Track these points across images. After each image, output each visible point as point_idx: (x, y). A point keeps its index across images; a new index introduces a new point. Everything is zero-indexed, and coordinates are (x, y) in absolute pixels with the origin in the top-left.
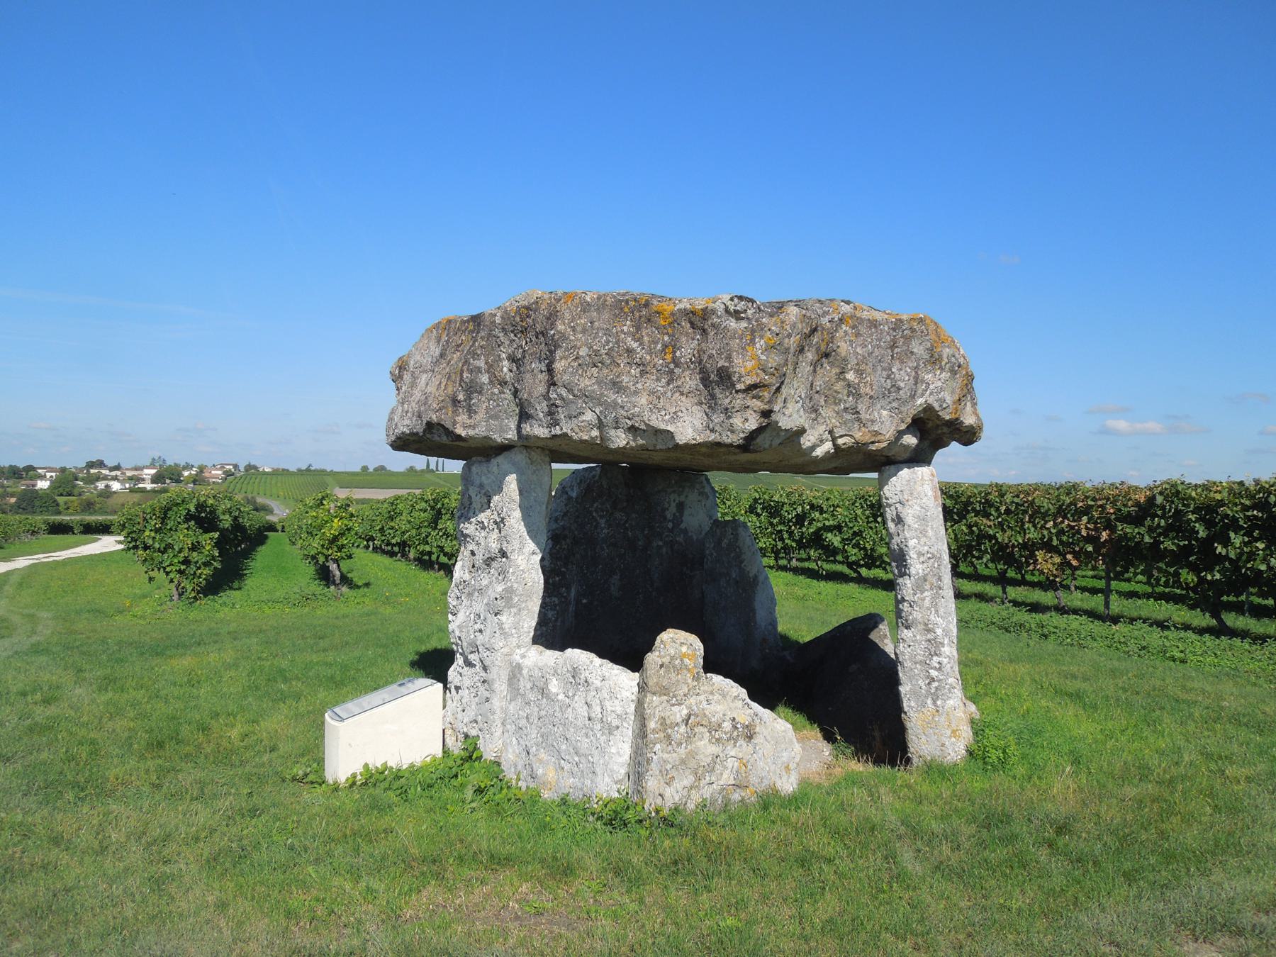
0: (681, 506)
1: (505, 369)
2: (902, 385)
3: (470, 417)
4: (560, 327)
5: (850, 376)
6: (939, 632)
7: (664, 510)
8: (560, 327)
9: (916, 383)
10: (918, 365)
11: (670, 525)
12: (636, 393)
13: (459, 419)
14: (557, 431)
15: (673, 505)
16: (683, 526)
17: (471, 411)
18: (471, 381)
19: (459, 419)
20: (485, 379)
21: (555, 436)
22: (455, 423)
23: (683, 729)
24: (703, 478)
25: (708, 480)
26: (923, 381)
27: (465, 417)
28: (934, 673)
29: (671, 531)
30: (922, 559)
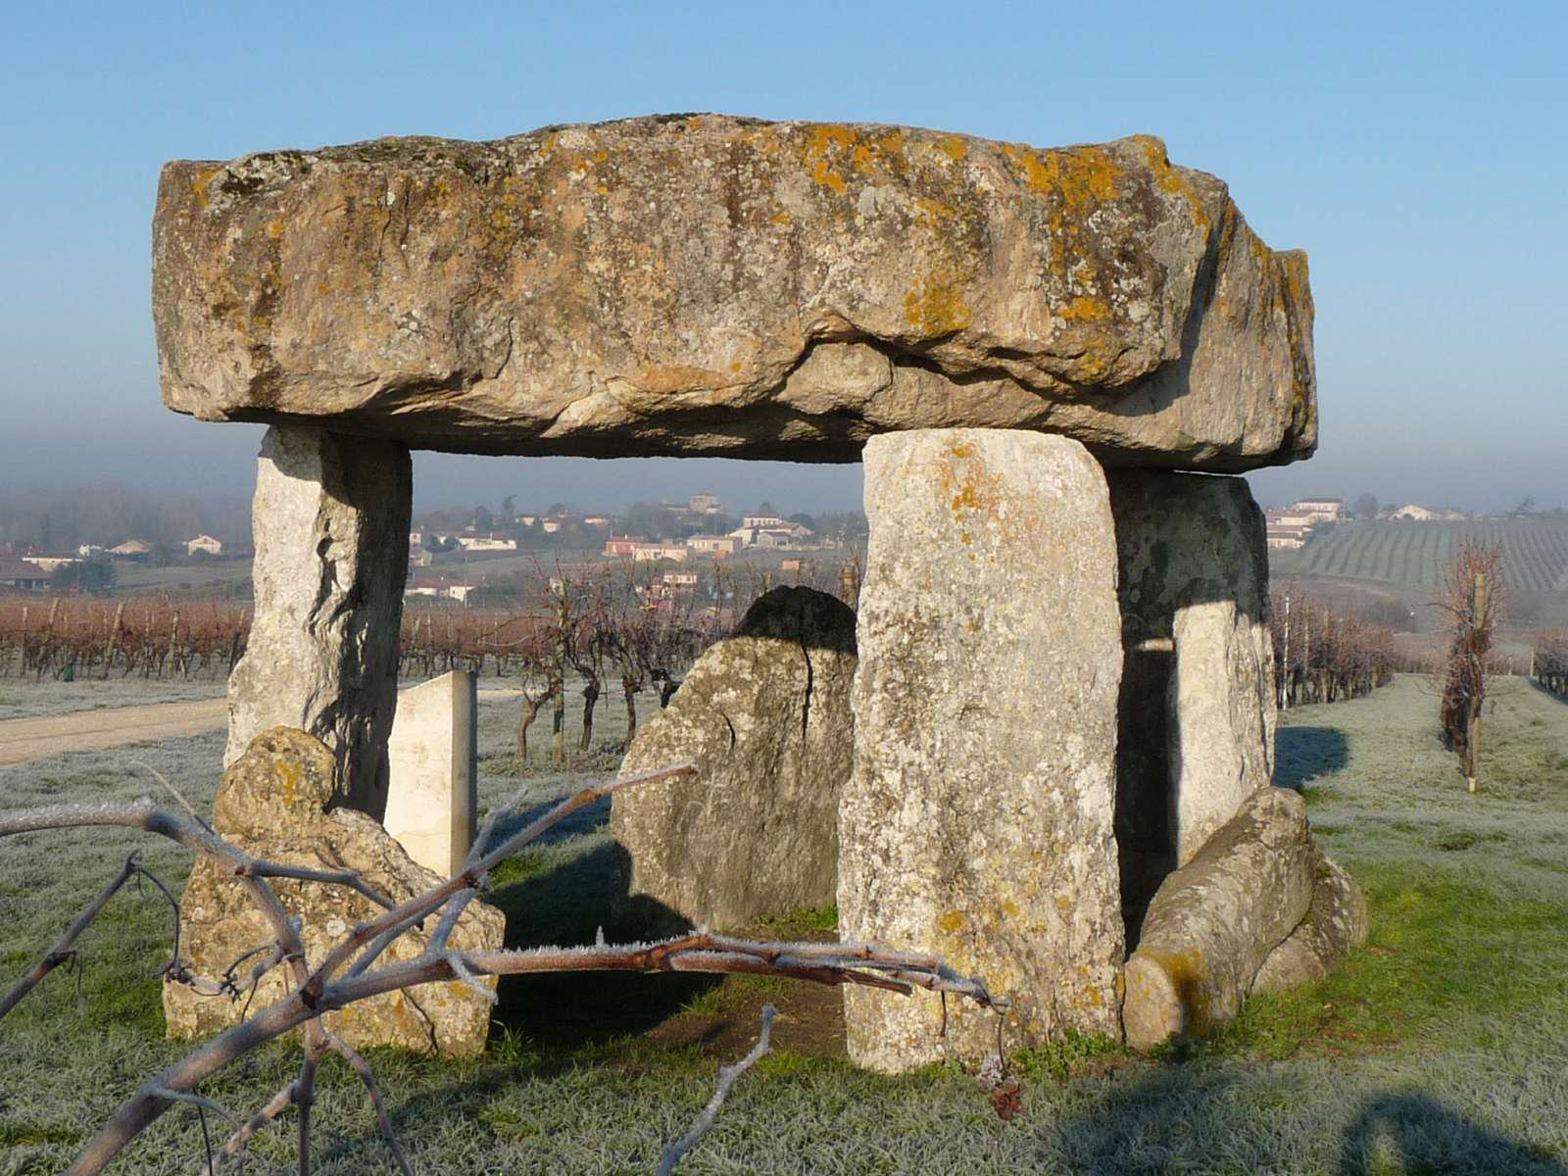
2: (760, 271)
5: (598, 265)
9: (795, 265)
10: (798, 228)
26: (812, 261)
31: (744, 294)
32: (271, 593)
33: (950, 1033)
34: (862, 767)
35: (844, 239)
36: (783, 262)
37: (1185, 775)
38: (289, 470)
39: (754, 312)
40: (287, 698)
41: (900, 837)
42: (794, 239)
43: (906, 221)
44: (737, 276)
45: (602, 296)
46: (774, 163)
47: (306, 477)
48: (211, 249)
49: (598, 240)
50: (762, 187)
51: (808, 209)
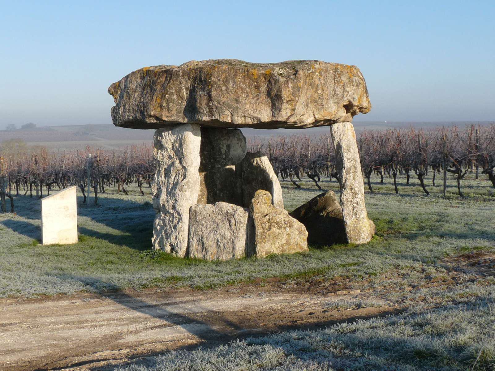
0: (229, 147)
1: (185, 93)
2: (339, 93)
3: (169, 113)
4: (213, 79)
5: (320, 91)
6: (356, 189)
7: (220, 149)
8: (213, 79)
9: (344, 92)
10: (344, 84)
11: (224, 156)
12: (245, 103)
13: (163, 113)
14: (214, 118)
15: (225, 146)
16: (230, 157)
17: (169, 110)
18: (169, 98)
19: (163, 113)
20: (175, 97)
21: (212, 120)
22: (161, 115)
23: (268, 224)
24: (239, 131)
25: (241, 132)
26: (346, 91)
27: (167, 112)
28: (355, 205)
29: (225, 159)
30: (349, 161)
31: (335, 97)
32: (192, 163)
33: (219, 254)
34: (349, 188)
35: (352, 87)
36: (342, 91)
37: (274, 192)
38: (194, 134)
39: (336, 101)
40: (196, 187)
41: (359, 200)
42: (344, 86)
43: (360, 84)
44: (335, 94)
45: (319, 98)
46: (341, 72)
47: (198, 136)
48: (286, 88)
49: (320, 86)
50: (339, 77)
51: (347, 81)
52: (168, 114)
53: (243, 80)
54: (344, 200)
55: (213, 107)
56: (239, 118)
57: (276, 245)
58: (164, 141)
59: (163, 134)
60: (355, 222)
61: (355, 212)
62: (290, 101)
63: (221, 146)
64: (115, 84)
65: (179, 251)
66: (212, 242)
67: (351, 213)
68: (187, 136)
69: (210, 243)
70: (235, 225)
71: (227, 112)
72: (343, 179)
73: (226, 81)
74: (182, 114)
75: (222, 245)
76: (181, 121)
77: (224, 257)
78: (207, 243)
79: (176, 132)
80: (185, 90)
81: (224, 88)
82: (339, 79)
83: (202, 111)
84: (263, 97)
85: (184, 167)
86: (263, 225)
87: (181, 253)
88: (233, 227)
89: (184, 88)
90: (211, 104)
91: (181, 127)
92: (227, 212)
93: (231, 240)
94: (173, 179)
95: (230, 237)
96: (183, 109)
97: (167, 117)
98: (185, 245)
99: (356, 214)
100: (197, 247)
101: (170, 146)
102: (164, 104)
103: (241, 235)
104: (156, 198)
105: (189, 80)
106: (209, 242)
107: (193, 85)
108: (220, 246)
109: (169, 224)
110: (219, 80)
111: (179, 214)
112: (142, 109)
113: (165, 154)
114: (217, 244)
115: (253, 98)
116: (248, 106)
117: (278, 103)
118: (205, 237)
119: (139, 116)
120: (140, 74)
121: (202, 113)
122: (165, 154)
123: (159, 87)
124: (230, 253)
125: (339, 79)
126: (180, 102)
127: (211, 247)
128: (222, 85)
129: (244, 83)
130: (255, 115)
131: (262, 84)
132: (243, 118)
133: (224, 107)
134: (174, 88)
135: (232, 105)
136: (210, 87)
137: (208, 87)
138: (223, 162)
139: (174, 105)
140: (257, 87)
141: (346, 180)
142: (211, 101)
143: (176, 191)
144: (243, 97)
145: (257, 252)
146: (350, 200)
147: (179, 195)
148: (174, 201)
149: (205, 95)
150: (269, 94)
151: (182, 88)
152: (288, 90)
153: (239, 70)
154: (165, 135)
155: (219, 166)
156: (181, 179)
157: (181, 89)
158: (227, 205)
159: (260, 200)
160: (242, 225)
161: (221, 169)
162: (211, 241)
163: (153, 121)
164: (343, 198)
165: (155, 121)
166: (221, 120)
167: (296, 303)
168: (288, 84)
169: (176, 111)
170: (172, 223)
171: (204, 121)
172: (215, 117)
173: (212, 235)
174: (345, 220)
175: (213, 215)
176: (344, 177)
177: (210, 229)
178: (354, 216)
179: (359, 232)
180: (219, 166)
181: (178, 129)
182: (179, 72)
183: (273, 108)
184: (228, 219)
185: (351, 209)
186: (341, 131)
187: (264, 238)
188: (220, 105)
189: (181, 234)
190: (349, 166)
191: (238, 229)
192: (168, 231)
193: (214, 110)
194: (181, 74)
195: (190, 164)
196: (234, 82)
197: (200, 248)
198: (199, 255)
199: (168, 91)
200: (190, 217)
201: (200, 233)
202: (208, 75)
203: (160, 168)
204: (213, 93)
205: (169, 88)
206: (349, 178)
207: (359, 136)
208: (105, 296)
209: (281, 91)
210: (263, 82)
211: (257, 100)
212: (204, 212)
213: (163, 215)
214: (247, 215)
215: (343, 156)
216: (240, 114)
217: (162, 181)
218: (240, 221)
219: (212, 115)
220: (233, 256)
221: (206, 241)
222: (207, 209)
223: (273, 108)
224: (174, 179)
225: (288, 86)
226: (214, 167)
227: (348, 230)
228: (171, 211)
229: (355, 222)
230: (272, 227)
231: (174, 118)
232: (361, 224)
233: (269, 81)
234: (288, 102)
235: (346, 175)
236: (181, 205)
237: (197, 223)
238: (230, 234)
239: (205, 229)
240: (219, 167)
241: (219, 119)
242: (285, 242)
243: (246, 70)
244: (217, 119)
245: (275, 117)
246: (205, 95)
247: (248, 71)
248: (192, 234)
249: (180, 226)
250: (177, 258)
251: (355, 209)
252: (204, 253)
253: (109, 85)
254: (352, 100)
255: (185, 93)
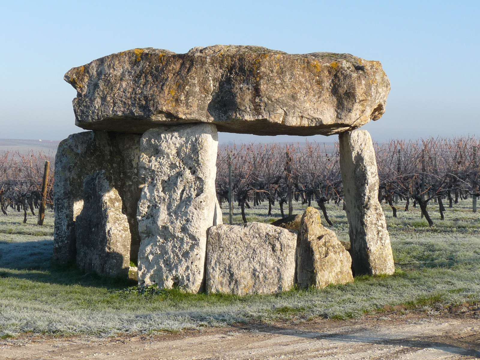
1: (212, 85)
4: (263, 69)
7: (131, 161)
10: (377, 84)
11: (136, 171)
12: (305, 101)
14: (260, 117)
17: (187, 105)
20: (197, 89)
22: (177, 112)
23: (324, 248)
26: (379, 92)
27: (185, 108)
28: (380, 228)
46: (377, 69)
52: (187, 111)
53: (302, 73)
54: (368, 222)
55: (262, 104)
56: (294, 119)
57: (333, 274)
58: (164, 145)
59: (163, 135)
60: (381, 248)
61: (380, 237)
62: (363, 100)
63: (132, 158)
64: (78, 68)
65: (190, 285)
66: (246, 272)
67: (376, 237)
68: (206, 140)
69: (244, 274)
70: (281, 250)
71: (280, 111)
72: (366, 197)
73: (281, 72)
74: (205, 112)
75: (261, 276)
76: (204, 119)
77: (264, 290)
78: (238, 273)
79: (185, 135)
80: (212, 82)
81: (278, 82)
82: (374, 77)
83: (243, 108)
84: (327, 95)
85: (198, 179)
86: (320, 249)
87: (195, 287)
88: (278, 253)
89: (210, 78)
90: (257, 100)
91: (194, 128)
92: (268, 234)
93: (276, 268)
94: (179, 194)
95: (274, 265)
96: (207, 105)
97: (185, 114)
98: (200, 278)
99: (381, 239)
100: (221, 279)
101: (174, 152)
102: (183, 98)
103: (289, 262)
104: (144, 218)
105: (221, 68)
106: (242, 272)
107: (227, 76)
108: (258, 277)
109: (173, 252)
110: (272, 71)
111: (193, 238)
112: (144, 103)
113: (164, 161)
114: (254, 274)
115: (314, 96)
116: (308, 105)
117: (348, 103)
118: (235, 266)
119: (137, 112)
120: (130, 58)
121: (243, 111)
122: (164, 161)
123: (170, 75)
124: (274, 285)
125: (374, 77)
126: (203, 96)
127: (244, 278)
128: (276, 78)
129: (303, 76)
130: (316, 116)
131: (325, 79)
132: (299, 119)
133: (278, 104)
134: (196, 78)
135: (288, 102)
136: (258, 79)
137: (256, 79)
138: (134, 178)
139: (195, 99)
140: (319, 83)
141: (369, 199)
142: (259, 96)
143: (189, 209)
144: (301, 93)
145: (317, 282)
146: (374, 222)
147: (193, 213)
148: (184, 222)
149: (249, 89)
150: (335, 91)
151: (208, 78)
152: (361, 87)
153: (297, 60)
154: (165, 138)
155: (131, 183)
156: (194, 194)
157: (206, 80)
158: (266, 226)
159: (314, 219)
160: (290, 250)
161: (133, 188)
162: (244, 271)
163: (162, 118)
164: (367, 221)
165: (164, 119)
166: (271, 120)
167: (413, 339)
168: (361, 81)
169: (198, 106)
170: (179, 251)
171: (246, 120)
172: (263, 116)
173: (246, 263)
174: (368, 246)
175: (246, 238)
176: (367, 194)
177: (242, 256)
178: (379, 242)
179: (385, 260)
180: (131, 183)
181: (189, 130)
182: (206, 58)
183: (338, 109)
184: (270, 243)
185: (375, 233)
186: (362, 140)
187: (324, 265)
188: (272, 101)
189: (195, 264)
190: (373, 182)
191: (285, 255)
192: (172, 261)
193: (262, 108)
194: (208, 60)
195: (208, 175)
196: (292, 75)
197: (225, 280)
198: (224, 289)
199: (189, 82)
200: (207, 242)
201: (227, 262)
202: (255, 63)
203: (153, 179)
204: (263, 87)
205: (190, 78)
206: (373, 196)
207: (224, 154)
208: (258, 329)
209: (354, 89)
210: (327, 77)
211: (319, 98)
212: (233, 235)
213: (161, 240)
214: (296, 238)
215: (365, 170)
216: (297, 114)
217: (160, 197)
218: (288, 246)
219: (259, 114)
220: (280, 288)
221: (237, 271)
222: (237, 231)
223: (338, 109)
224: (182, 193)
225: (361, 83)
226: (125, 184)
227: (371, 258)
228: (180, 235)
229: (381, 248)
230: (330, 252)
231: (195, 116)
232: (387, 251)
233: (336, 76)
234: (360, 101)
235: (370, 192)
236: (197, 226)
237: (221, 249)
238: (273, 261)
239: (234, 256)
240: (129, 185)
241: (268, 119)
242: (339, 270)
243: (306, 61)
244: (266, 119)
245: (340, 119)
246: (249, 89)
247: (308, 63)
248: (213, 262)
249: (195, 253)
250: (187, 296)
251: (380, 234)
252: (232, 286)
253: (66, 69)
254: (383, 103)
255: (212, 85)
